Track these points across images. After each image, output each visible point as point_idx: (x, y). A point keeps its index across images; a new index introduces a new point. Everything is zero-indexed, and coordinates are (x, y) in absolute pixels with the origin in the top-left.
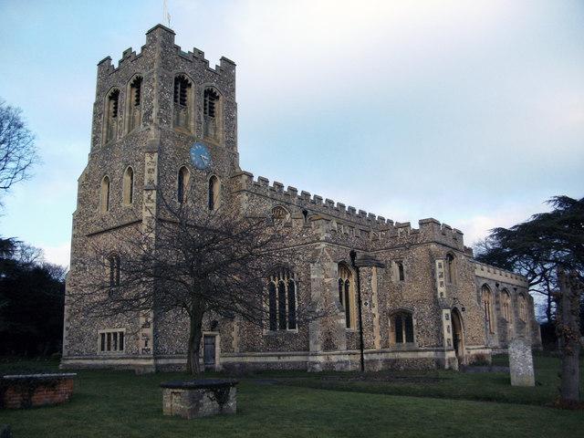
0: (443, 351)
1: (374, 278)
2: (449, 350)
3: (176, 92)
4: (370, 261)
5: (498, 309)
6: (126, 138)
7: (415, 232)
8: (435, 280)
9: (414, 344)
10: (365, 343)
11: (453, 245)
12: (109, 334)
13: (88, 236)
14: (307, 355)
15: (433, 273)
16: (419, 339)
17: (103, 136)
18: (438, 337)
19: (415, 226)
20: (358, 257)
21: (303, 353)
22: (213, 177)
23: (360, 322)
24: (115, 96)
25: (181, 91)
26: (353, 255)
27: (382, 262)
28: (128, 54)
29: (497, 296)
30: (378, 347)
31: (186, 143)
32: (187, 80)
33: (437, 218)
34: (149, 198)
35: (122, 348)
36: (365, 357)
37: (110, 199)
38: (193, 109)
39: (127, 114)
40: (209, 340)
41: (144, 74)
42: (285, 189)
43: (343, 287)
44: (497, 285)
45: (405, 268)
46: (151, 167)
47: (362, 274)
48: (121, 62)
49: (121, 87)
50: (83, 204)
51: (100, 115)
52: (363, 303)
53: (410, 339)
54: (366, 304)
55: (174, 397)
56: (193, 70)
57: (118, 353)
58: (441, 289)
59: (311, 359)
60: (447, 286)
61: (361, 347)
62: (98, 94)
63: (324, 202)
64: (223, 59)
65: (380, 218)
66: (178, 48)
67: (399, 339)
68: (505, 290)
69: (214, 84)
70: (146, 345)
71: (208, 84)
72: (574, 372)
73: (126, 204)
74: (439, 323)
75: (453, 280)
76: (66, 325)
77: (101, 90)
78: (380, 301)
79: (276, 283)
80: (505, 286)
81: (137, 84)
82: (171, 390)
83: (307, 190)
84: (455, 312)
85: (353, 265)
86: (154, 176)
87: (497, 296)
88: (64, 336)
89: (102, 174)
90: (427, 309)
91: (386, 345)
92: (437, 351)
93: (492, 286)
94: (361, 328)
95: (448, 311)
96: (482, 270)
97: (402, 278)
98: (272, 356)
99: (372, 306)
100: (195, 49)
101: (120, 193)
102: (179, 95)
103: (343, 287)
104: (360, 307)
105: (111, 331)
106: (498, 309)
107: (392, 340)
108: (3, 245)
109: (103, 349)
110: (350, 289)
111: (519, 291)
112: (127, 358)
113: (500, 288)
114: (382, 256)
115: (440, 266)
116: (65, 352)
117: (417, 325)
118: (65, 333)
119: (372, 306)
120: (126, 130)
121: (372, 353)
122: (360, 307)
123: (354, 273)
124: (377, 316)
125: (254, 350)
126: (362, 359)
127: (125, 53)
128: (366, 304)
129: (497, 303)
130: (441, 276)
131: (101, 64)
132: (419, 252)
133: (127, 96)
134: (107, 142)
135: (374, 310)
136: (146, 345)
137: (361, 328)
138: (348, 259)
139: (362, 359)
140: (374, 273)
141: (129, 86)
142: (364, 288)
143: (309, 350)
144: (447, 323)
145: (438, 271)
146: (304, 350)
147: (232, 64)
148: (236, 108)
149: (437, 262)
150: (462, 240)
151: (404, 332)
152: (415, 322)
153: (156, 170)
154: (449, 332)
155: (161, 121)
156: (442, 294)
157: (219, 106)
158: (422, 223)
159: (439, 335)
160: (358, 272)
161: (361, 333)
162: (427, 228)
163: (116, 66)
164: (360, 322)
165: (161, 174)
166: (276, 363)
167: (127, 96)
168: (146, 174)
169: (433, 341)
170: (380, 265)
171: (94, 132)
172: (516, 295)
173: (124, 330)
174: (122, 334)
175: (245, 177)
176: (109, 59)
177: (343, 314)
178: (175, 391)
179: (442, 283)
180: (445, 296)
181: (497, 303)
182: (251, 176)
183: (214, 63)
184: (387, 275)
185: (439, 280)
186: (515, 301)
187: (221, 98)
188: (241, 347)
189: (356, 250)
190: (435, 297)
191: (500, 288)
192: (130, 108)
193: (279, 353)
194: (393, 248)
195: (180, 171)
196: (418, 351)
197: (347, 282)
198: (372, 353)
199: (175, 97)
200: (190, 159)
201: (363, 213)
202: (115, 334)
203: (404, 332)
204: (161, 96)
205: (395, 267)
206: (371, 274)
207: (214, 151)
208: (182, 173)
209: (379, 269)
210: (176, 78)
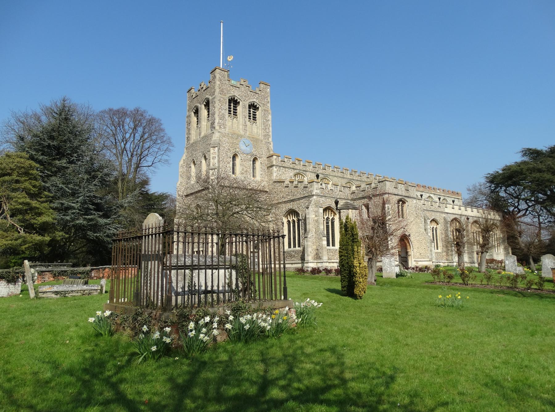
3: (230, 108)
26: (337, 203)
27: (357, 206)
32: (237, 100)
34: (213, 174)
38: (241, 117)
43: (434, 231)
44: (468, 219)
46: (214, 156)
56: (240, 93)
69: (255, 100)
71: (251, 100)
72: (62, 204)
79: (291, 220)
81: (207, 105)
86: (216, 161)
102: (232, 110)
103: (434, 231)
108: (554, 256)
113: (471, 220)
114: (357, 203)
153: (217, 157)
160: (340, 213)
165: (221, 159)
166: (290, 268)
177: (325, 238)
187: (260, 108)
189: (338, 200)
193: (292, 262)
194: (363, 198)
197: (333, 219)
199: (230, 111)
204: (220, 112)
208: (234, 157)
209: (354, 211)
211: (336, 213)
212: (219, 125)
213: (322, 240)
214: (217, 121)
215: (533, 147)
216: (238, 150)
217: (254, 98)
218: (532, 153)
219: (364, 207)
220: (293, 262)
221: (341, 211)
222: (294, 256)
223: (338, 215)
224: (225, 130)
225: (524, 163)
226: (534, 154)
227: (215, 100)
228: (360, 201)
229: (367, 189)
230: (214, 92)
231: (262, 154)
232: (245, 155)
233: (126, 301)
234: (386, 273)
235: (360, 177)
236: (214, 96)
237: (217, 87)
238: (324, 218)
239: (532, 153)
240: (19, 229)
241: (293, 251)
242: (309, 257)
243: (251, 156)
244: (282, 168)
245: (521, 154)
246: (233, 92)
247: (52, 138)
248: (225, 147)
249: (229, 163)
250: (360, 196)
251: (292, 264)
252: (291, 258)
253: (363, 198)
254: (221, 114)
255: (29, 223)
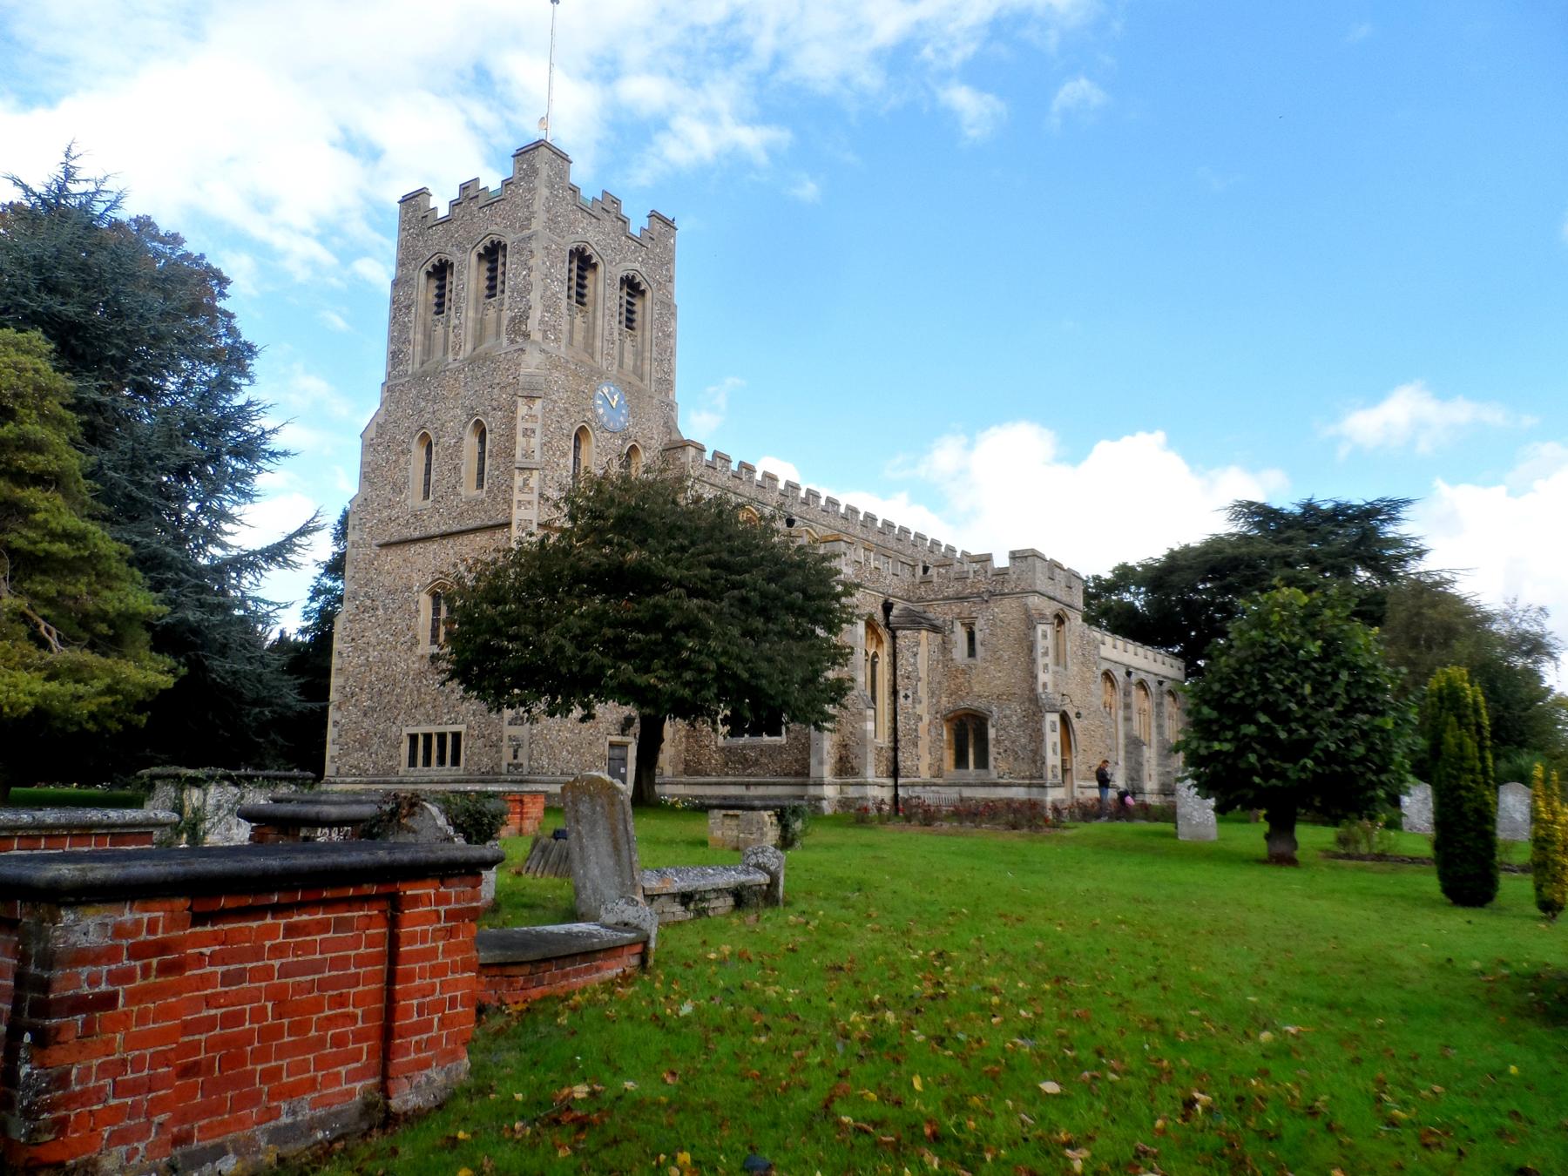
0: (1043, 786)
1: (923, 650)
2: (1055, 786)
4: (916, 621)
5: (1128, 719)
6: (471, 361)
7: (1003, 572)
8: (1034, 661)
9: (989, 774)
10: (901, 765)
11: (1064, 599)
12: (428, 737)
13: (381, 546)
14: (805, 784)
15: (1031, 648)
16: (998, 763)
17: (415, 351)
18: (1035, 762)
19: (1001, 561)
20: (895, 612)
21: (792, 780)
22: (633, 448)
23: (895, 730)
24: (440, 272)
25: (579, 276)
26: (887, 608)
28: (469, 192)
29: (1127, 694)
30: (925, 775)
31: (589, 379)
32: (590, 257)
33: (1040, 549)
35: (456, 761)
36: (901, 792)
37: (433, 478)
39: (471, 314)
40: (617, 752)
41: (509, 239)
42: (758, 476)
44: (1129, 674)
45: (978, 636)
46: (529, 425)
47: (901, 642)
48: (454, 205)
49: (455, 257)
50: (372, 484)
51: (408, 307)
52: (902, 694)
53: (982, 762)
54: (906, 697)
55: (727, 821)
56: (601, 237)
57: (448, 770)
58: (1043, 677)
59: (812, 791)
60: (1056, 673)
61: (895, 773)
62: (401, 264)
63: (823, 502)
64: (654, 215)
65: (917, 535)
66: (574, 190)
67: (961, 761)
68: (1142, 685)
69: (637, 266)
70: (515, 757)
73: (468, 490)
74: (1038, 737)
75: (1062, 661)
76: (333, 715)
77: (406, 258)
78: (932, 694)
80: (1143, 675)
81: (492, 254)
82: (724, 812)
83: (813, 487)
84: (1065, 719)
85: (887, 625)
87: (1127, 694)
88: (329, 738)
89: (415, 428)
90: (1015, 711)
91: (939, 773)
92: (1029, 786)
93: (1120, 675)
94: (896, 741)
95: (1056, 717)
96: (1115, 647)
97: (972, 652)
98: (735, 784)
99: (917, 701)
100: (605, 193)
101: (456, 469)
104: (895, 701)
105: (434, 729)
106: (1128, 719)
107: (949, 757)
109: (412, 762)
110: (879, 668)
111: (1167, 685)
112: (467, 782)
114: (937, 613)
115: (1045, 636)
116: (330, 769)
117: (998, 741)
118: (332, 733)
119: (917, 701)
120: (469, 347)
121: (913, 785)
122: (895, 701)
123: (886, 638)
124: (926, 719)
125: (698, 773)
126: (896, 795)
127: (464, 188)
128: (906, 697)
129: (1127, 706)
130: (1046, 654)
131: (405, 200)
132: (1007, 610)
133: (469, 277)
134: (422, 364)
135: (922, 709)
136: (515, 757)
137: (896, 741)
138: (879, 616)
139: (896, 795)
140: (924, 642)
141: (474, 258)
142: (904, 665)
143: (808, 775)
144: (1053, 738)
145: (1041, 644)
146: (797, 774)
147: (669, 224)
148: (674, 314)
149: (1040, 628)
150: (567, 172)
151: (971, 751)
152: (992, 733)
154: (1054, 752)
155: (545, 337)
156: (1045, 685)
157: (646, 308)
158: (1014, 556)
159: (1037, 757)
160: (894, 638)
161: (895, 749)
162: (1022, 565)
163: (443, 211)
164: (895, 730)
167: (469, 277)
168: (520, 438)
169: (1025, 769)
170: (935, 629)
171: (392, 339)
172: (1161, 695)
173: (462, 728)
174: (457, 736)
175: (692, 451)
176: (423, 192)
178: (731, 812)
179: (1046, 666)
180: (1050, 689)
181: (1127, 706)
182: (701, 450)
183: (638, 223)
184: (945, 647)
185: (1041, 661)
186: (1159, 705)
188: (675, 767)
189: (892, 600)
190: (1033, 690)
191: (1134, 678)
192: (477, 301)
194: (960, 598)
195: (576, 434)
196: (996, 785)
198: (913, 785)
200: (594, 411)
201: (888, 525)
202: (442, 737)
203: (971, 751)
204: (546, 288)
205: (960, 634)
206: (918, 644)
207: (634, 396)
208: (580, 435)
209: (932, 635)
210: (571, 252)
211: (884, 638)
212: (542, 327)
213: (865, 719)
214: (536, 315)
215: (1260, 498)
216: (589, 415)
217: (636, 259)
218: (1253, 514)
219: (958, 624)
220: (752, 780)
221: (899, 633)
222: (756, 763)
223: (886, 646)
224: (559, 347)
225: (1243, 538)
226: (1263, 515)
227: (534, 245)
228: (946, 608)
229: (971, 575)
230: (529, 219)
231: (651, 438)
232: (607, 435)
233: (72, 899)
234: (1190, 825)
235: (882, 537)
236: (526, 232)
237: (538, 205)
238: (867, 654)
239: (1253, 514)
240: (42, 629)
241: (753, 748)
242: (873, 770)
243: (624, 440)
244: (708, 486)
245: (1226, 515)
246: (583, 228)
247: (50, 287)
248: (556, 402)
249: (565, 455)
250: (950, 592)
251: (748, 785)
252: (744, 769)
253: (960, 598)
254: (549, 293)
255: (1396, 588)
